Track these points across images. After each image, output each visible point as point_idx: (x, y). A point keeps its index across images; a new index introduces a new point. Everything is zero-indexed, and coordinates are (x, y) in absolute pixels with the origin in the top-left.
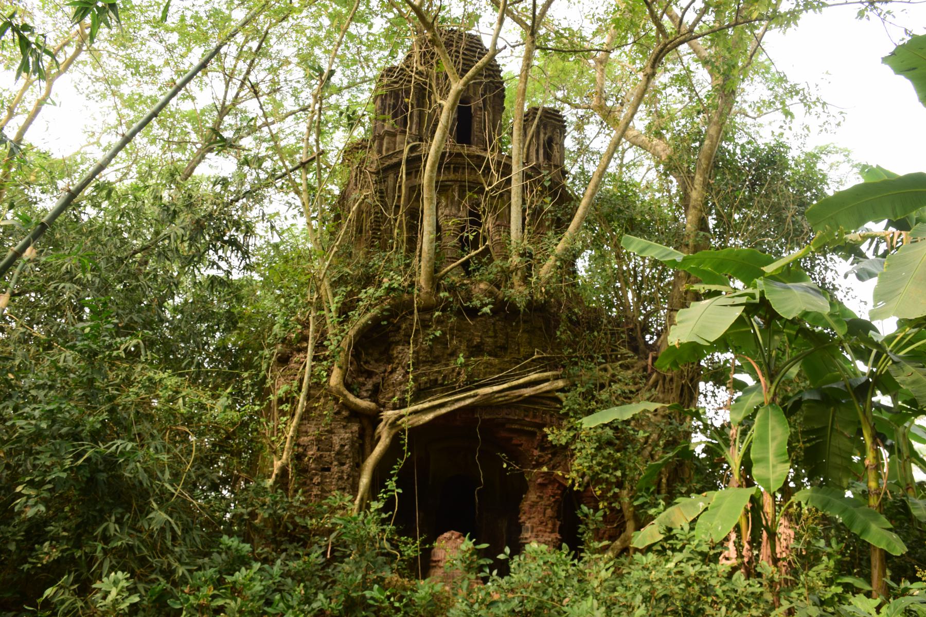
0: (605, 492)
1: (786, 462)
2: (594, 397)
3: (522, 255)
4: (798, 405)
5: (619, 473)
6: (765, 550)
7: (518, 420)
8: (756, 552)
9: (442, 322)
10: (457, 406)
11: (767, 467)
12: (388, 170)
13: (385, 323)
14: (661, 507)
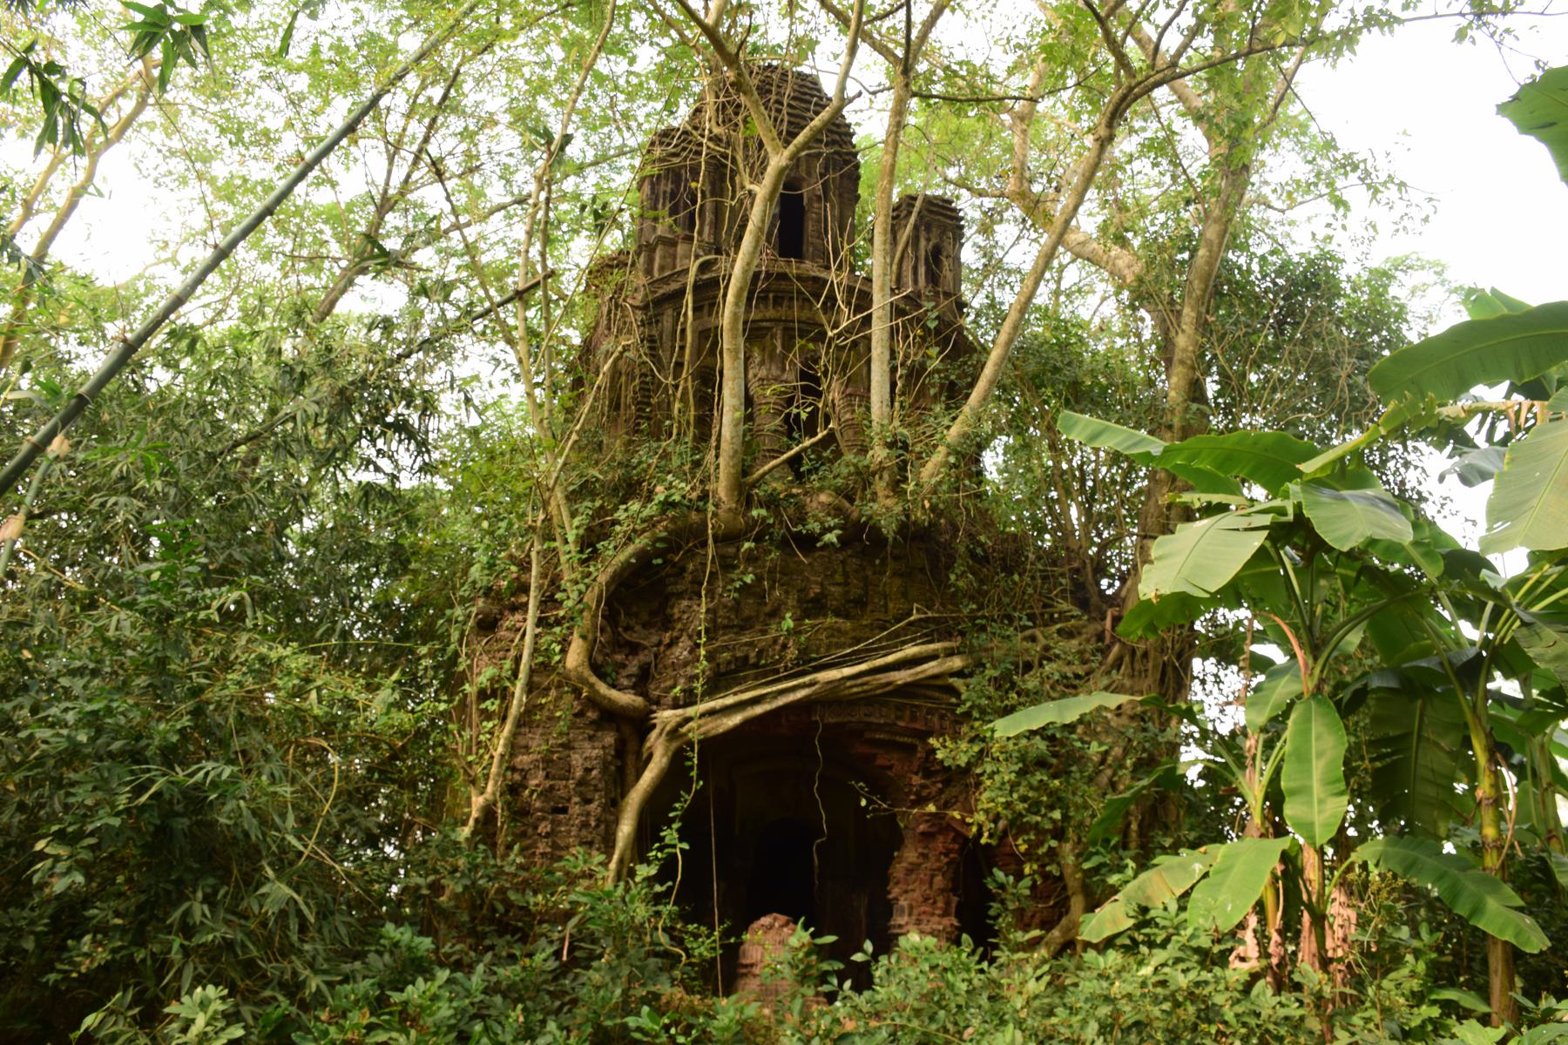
0: (1033, 846)
1: (1341, 793)
2: (1013, 684)
3: (891, 446)
4: (1360, 696)
5: (1057, 815)
6: (1308, 944)
7: (886, 724)
8: (1291, 948)
9: (756, 559)
10: (781, 701)
11: (1310, 804)
12: (662, 303)
13: (659, 561)
14: (1130, 872)
